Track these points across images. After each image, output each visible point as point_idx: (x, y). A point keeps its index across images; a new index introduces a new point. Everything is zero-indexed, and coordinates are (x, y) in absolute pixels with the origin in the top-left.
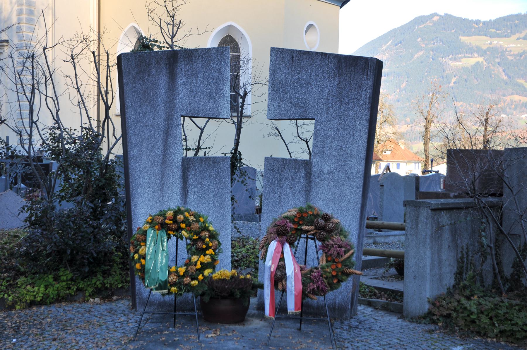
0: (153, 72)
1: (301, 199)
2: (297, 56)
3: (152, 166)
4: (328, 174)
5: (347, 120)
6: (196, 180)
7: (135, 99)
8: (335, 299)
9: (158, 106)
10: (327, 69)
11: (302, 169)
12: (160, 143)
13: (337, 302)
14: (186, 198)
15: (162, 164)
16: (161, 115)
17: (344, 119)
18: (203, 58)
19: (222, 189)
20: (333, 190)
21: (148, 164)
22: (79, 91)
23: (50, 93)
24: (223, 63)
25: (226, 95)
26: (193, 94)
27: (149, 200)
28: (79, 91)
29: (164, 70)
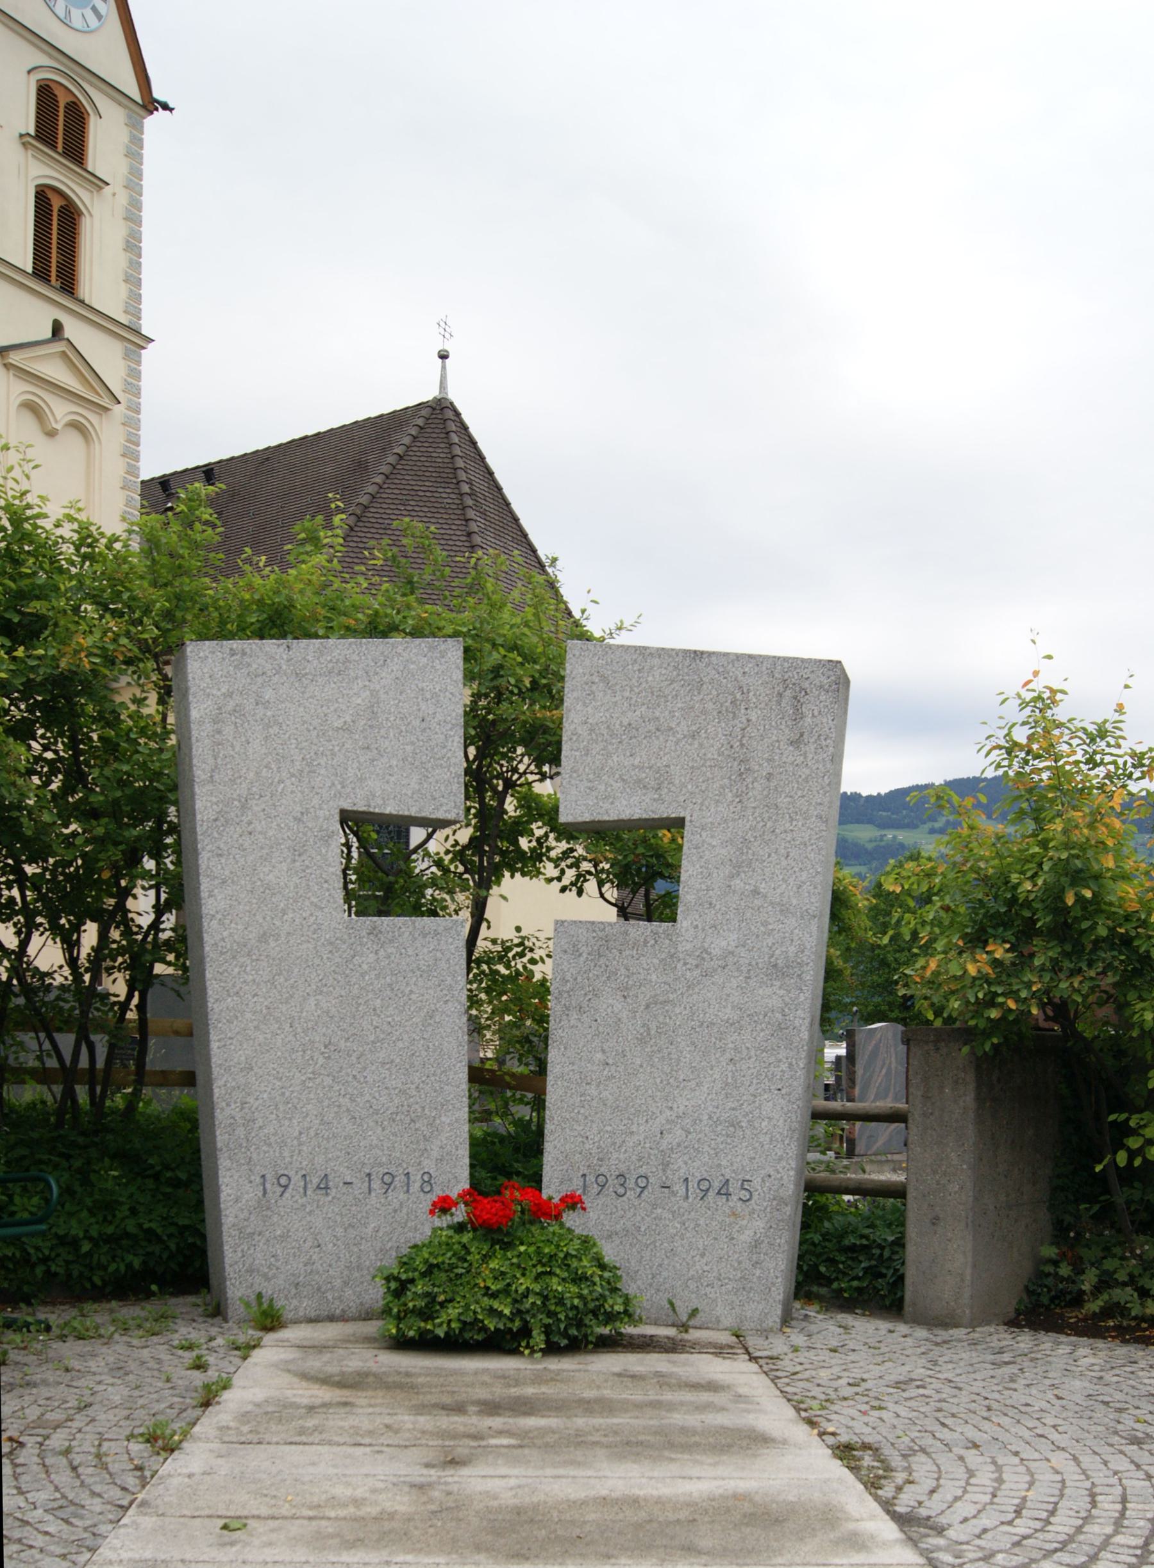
5: (770, 818)
19: (446, 1002)
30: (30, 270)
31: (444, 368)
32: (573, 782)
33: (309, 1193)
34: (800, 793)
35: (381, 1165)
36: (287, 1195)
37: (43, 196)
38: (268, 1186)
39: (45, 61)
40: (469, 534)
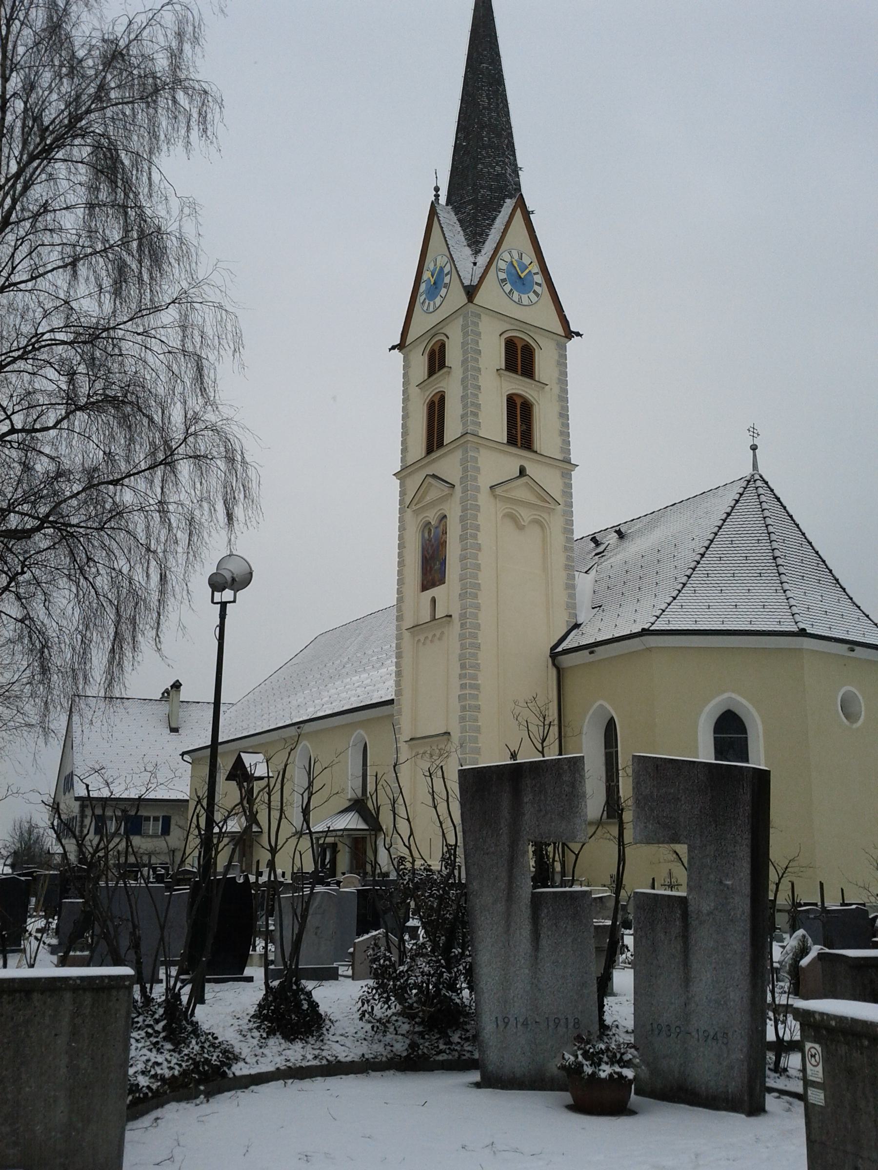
1: (679, 948)
8: (727, 1086)
14: (537, 944)
15: (507, 900)
24: (577, 775)
26: (542, 813)
27: (492, 945)
30: (505, 441)
31: (755, 455)
37: (511, 400)
39: (508, 327)
40: (775, 558)
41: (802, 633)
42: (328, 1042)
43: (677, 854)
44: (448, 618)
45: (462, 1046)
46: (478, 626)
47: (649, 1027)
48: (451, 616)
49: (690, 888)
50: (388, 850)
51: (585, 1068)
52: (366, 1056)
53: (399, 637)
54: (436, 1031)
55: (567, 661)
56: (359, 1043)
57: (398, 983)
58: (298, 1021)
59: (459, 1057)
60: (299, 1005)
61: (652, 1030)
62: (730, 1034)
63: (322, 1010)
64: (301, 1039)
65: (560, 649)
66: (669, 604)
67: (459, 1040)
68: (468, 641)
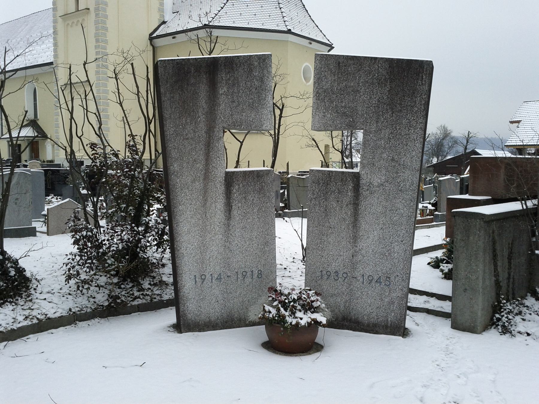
0: (192, 81)
2: (343, 62)
3: (193, 181)
4: (379, 187)
6: (240, 194)
7: (173, 110)
8: (386, 316)
9: (199, 117)
10: (376, 75)
11: (349, 181)
12: (202, 157)
13: (389, 319)
15: (204, 179)
16: (202, 126)
17: (396, 127)
18: (244, 66)
19: (267, 203)
20: (384, 203)
21: (189, 179)
22: (121, 106)
23: (92, 107)
24: (265, 72)
25: (269, 105)
28: (121, 106)
29: (204, 78)
32: (317, 113)
33: (213, 281)
34: (412, 118)
35: (242, 268)
36: (205, 282)
38: (197, 279)
41: (289, 32)
42: (37, 301)
43: (315, 141)
44: (87, 10)
45: (152, 291)
46: (106, 17)
47: (319, 274)
48: (88, 9)
49: (363, 166)
50: (80, 138)
51: (287, 318)
52: (73, 310)
53: (55, 22)
54: (129, 280)
55: (158, 42)
56: (64, 299)
57: (101, 250)
58: (7, 286)
59: (151, 300)
60: (6, 273)
61: (322, 276)
62: (392, 278)
63: (28, 274)
64: (11, 302)
65: (155, 35)
66: (219, 11)
67: (150, 287)
68: (100, 25)
